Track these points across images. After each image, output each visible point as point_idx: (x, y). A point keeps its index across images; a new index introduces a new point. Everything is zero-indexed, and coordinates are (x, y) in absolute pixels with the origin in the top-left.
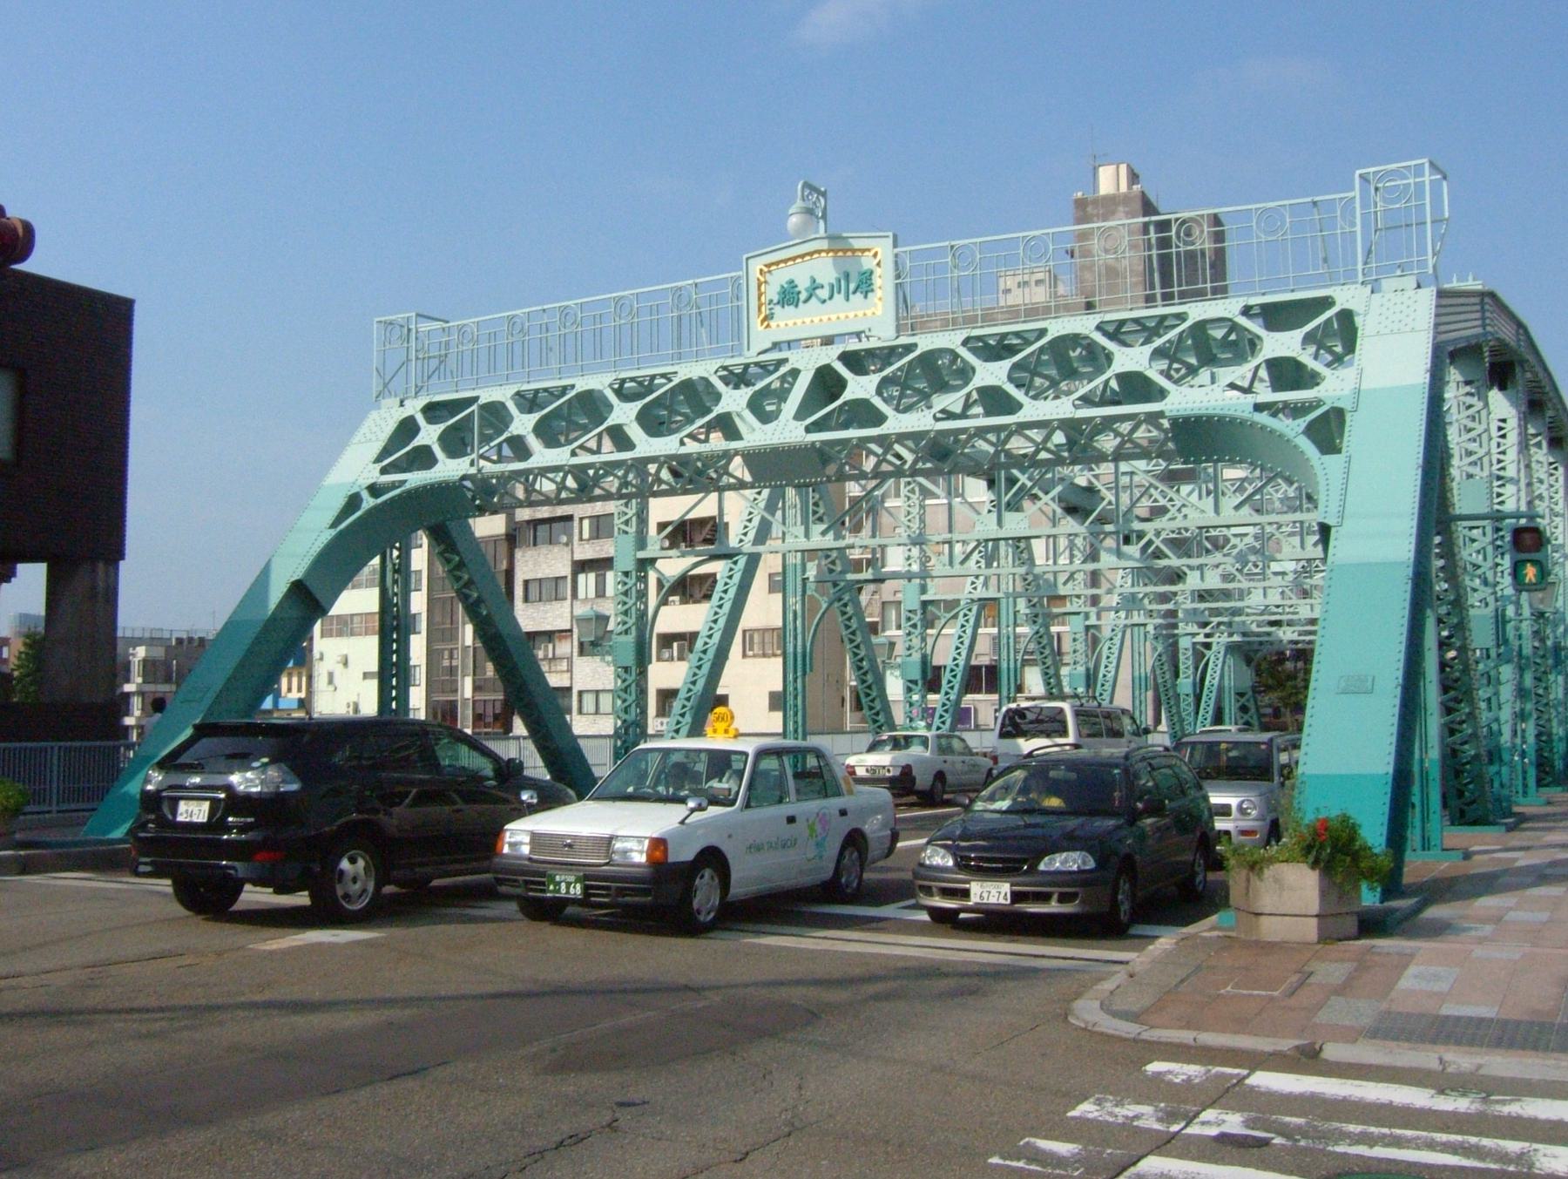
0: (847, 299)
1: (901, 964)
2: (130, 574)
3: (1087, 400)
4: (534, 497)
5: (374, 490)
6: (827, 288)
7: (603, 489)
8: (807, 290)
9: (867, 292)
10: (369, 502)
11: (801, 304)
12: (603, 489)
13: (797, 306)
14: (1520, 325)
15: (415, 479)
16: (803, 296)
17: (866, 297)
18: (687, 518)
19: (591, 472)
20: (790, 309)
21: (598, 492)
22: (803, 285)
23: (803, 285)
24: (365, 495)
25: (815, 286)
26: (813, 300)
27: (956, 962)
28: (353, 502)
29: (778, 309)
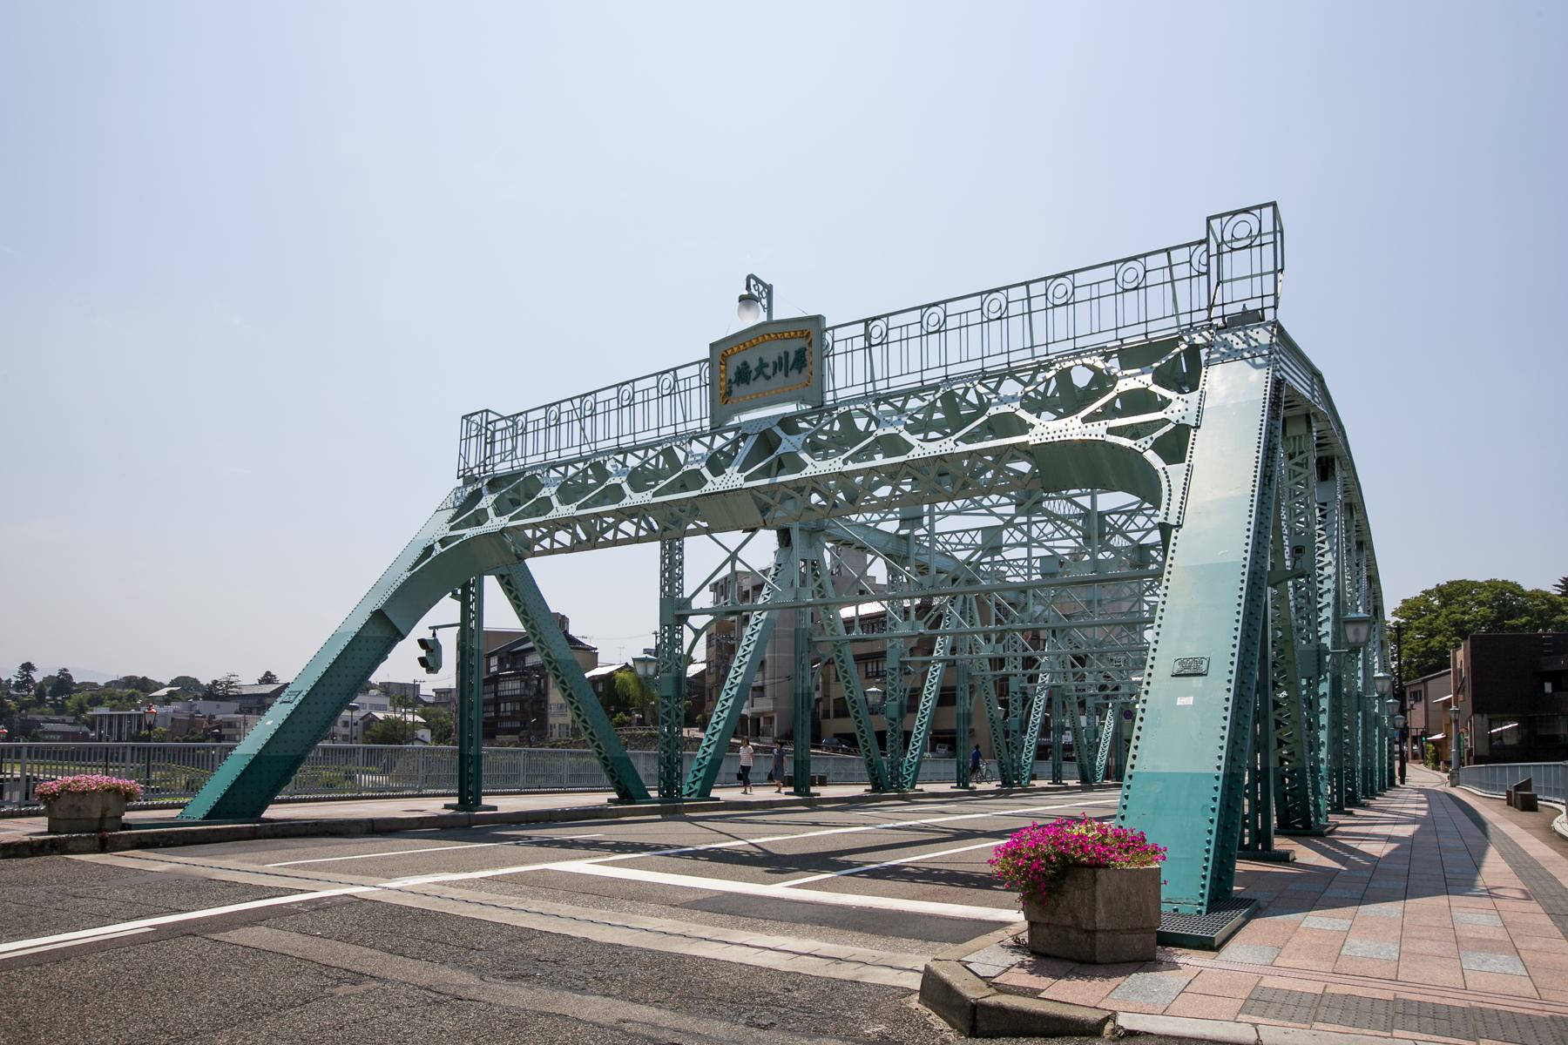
0: (786, 375)
1: (707, 895)
2: (426, 638)
3: (1110, 431)
4: (556, 546)
5: (443, 542)
6: (771, 365)
7: (542, 546)
8: (756, 369)
9: (801, 368)
10: (438, 549)
11: (751, 382)
12: (542, 546)
13: (748, 384)
14: (1316, 377)
15: (469, 533)
16: (754, 374)
17: (800, 372)
18: (1141, 543)
19: (859, 479)
20: (743, 386)
21: (537, 548)
22: (754, 364)
23: (754, 364)
24: (438, 546)
25: (762, 365)
26: (761, 378)
27: (779, 932)
28: (429, 550)
29: (734, 387)
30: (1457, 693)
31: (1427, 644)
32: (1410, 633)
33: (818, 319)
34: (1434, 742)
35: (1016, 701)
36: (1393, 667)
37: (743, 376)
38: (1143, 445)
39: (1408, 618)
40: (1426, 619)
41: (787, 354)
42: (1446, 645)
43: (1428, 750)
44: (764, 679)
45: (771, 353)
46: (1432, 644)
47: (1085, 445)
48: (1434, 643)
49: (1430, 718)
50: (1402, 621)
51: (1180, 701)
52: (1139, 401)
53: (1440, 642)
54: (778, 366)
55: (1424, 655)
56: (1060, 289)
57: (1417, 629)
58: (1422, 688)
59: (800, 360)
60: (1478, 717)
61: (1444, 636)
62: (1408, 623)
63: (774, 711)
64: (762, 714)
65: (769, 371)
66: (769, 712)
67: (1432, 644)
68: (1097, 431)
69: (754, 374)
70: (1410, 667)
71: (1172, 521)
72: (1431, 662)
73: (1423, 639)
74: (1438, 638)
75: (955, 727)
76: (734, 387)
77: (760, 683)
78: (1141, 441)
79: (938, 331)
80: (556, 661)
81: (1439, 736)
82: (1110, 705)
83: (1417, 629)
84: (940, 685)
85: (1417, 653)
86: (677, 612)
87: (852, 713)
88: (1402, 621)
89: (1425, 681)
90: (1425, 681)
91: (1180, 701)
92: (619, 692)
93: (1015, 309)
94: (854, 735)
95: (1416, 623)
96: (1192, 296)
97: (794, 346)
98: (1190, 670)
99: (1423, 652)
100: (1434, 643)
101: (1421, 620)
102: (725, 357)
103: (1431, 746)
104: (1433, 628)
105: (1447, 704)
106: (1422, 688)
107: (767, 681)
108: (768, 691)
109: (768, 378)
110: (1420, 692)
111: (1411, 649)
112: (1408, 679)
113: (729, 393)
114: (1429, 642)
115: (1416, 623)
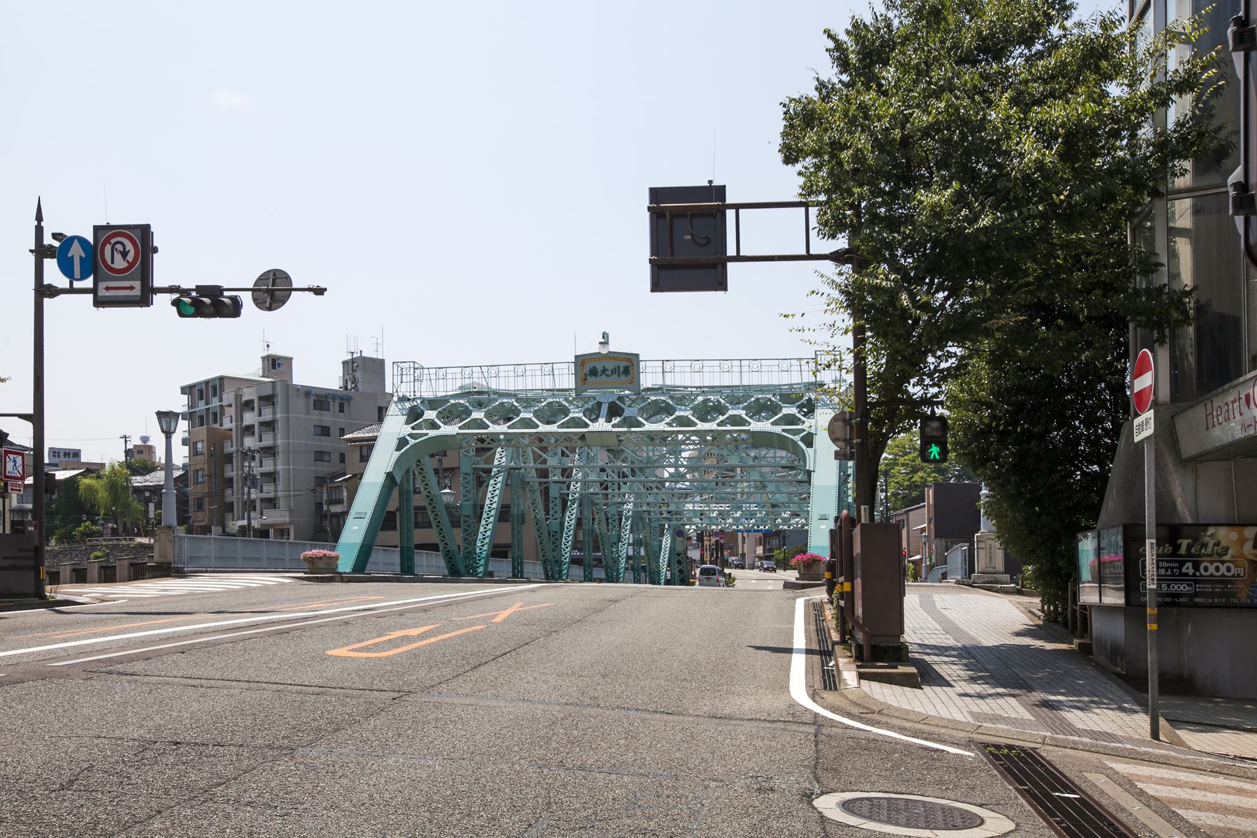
3: (783, 430)
16: (600, 373)
23: (600, 368)
29: (588, 377)
30: (929, 523)
31: (910, 479)
32: (897, 468)
33: (637, 355)
34: (913, 562)
35: (614, 521)
36: (882, 497)
37: (594, 372)
38: (797, 438)
39: (896, 455)
40: (911, 456)
41: (619, 367)
42: (926, 480)
43: (909, 568)
44: (276, 491)
45: (610, 365)
46: (914, 479)
47: (771, 434)
48: (916, 478)
49: (911, 539)
50: (891, 457)
51: (822, 527)
52: (791, 420)
53: (922, 478)
54: (614, 371)
55: (909, 488)
56: (755, 365)
57: (903, 465)
58: (905, 517)
59: (627, 371)
60: (939, 540)
61: (925, 472)
62: (895, 459)
63: (290, 523)
64: (272, 526)
65: (609, 373)
66: (285, 524)
67: (914, 479)
68: (778, 429)
69: (600, 373)
70: (896, 498)
71: (812, 469)
72: (914, 494)
73: (907, 474)
74: (921, 474)
75: (510, 542)
76: (588, 377)
77: (272, 495)
78: (796, 437)
79: (699, 372)
80: (434, 496)
81: (918, 557)
82: (666, 526)
83: (903, 465)
84: (501, 503)
85: (902, 485)
86: (474, 466)
87: (434, 524)
88: (891, 457)
89: (907, 512)
90: (907, 512)
91: (822, 527)
92: (83, 499)
93: (735, 369)
94: (437, 544)
95: (902, 460)
96: (808, 378)
97: (623, 364)
98: (823, 518)
99: (907, 486)
100: (916, 478)
101: (906, 458)
102: (583, 362)
103: (911, 565)
104: (915, 465)
105: (923, 530)
106: (905, 517)
107: (280, 494)
108: (282, 503)
109: (608, 376)
110: (903, 520)
111: (897, 483)
112: (895, 509)
113: (586, 379)
114: (912, 477)
115: (902, 460)
